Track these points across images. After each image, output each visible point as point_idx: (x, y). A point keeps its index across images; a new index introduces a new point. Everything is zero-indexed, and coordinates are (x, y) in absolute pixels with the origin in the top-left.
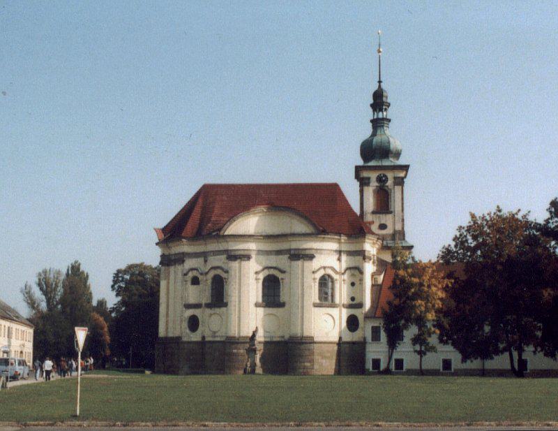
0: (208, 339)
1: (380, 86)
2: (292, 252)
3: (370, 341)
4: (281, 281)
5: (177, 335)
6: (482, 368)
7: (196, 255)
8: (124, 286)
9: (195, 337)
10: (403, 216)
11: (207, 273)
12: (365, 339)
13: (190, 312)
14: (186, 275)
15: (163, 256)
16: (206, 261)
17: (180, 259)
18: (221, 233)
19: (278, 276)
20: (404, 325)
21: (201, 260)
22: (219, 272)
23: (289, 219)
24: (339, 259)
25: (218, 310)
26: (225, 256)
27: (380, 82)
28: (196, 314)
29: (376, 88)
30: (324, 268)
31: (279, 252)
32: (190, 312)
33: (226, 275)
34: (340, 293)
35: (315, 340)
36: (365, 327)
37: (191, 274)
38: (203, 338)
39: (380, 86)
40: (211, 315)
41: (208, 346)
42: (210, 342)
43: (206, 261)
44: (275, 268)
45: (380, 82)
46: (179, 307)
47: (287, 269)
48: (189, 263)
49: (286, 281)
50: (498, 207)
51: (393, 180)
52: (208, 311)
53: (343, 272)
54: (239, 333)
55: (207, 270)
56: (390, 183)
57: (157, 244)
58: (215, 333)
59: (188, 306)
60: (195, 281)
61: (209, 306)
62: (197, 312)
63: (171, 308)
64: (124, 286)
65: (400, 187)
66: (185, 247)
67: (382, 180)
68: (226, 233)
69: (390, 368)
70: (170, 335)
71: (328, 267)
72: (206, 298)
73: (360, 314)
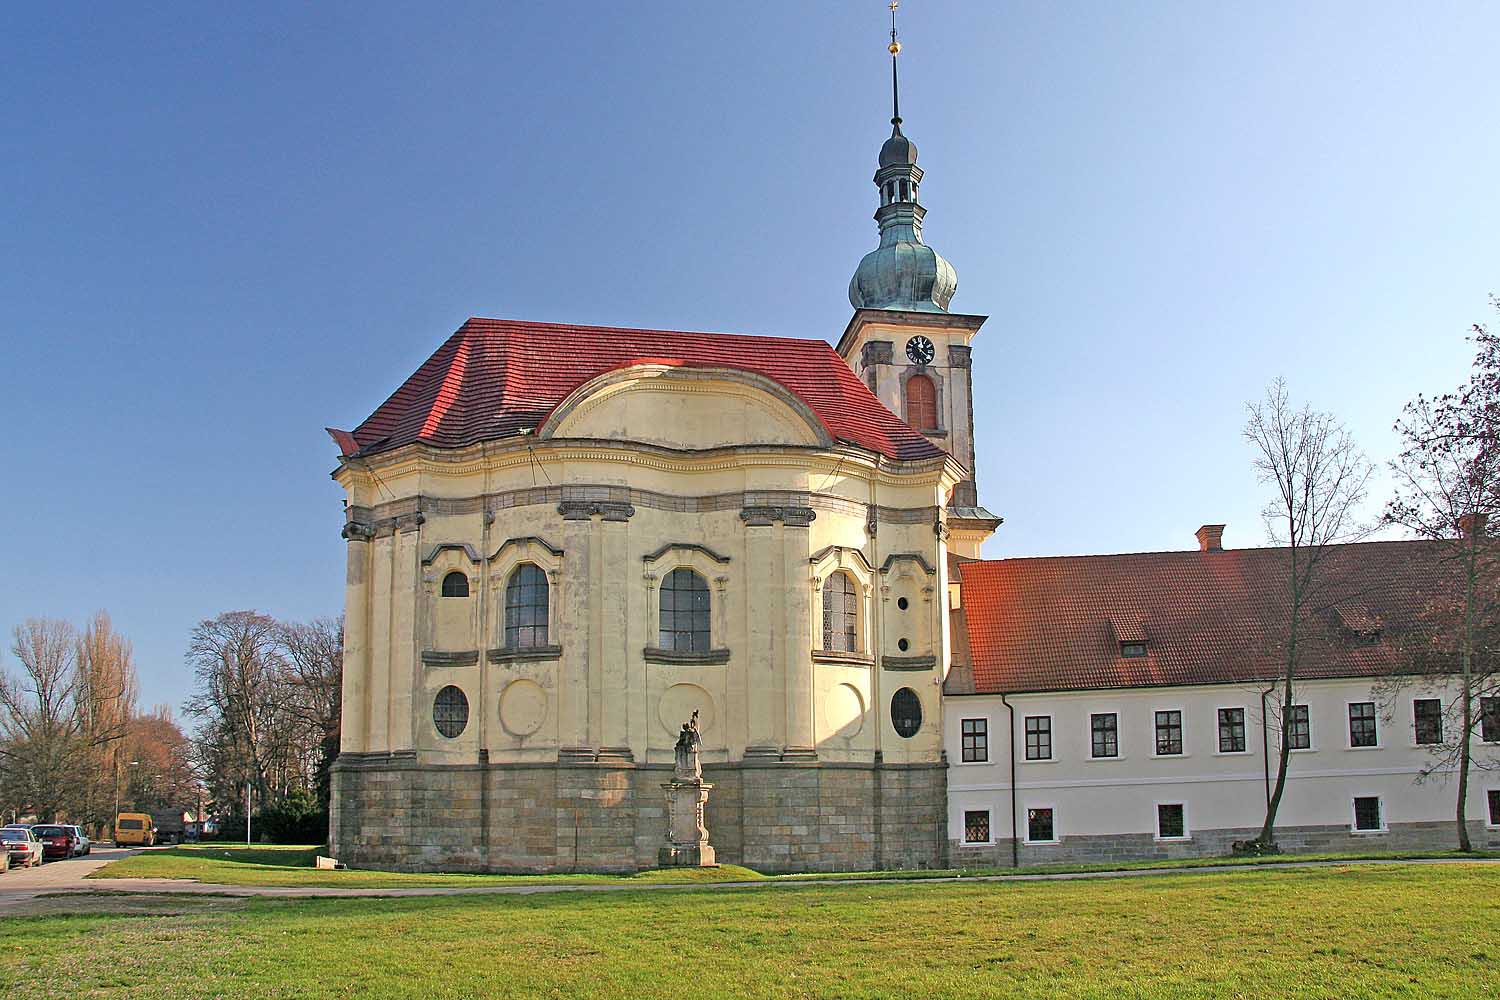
1: (897, 131)
2: (750, 501)
4: (713, 587)
8: (206, 830)
9: (461, 751)
13: (440, 678)
14: (426, 562)
16: (489, 523)
18: (543, 432)
22: (537, 555)
26: (553, 506)
27: (896, 121)
31: (707, 503)
32: (440, 678)
34: (272, 885)
36: (942, 723)
38: (484, 754)
39: (897, 131)
40: (508, 685)
41: (497, 777)
42: (508, 767)
43: (489, 523)
45: (896, 121)
48: (440, 529)
50: (1000, 521)
52: (498, 673)
56: (939, 360)
58: (521, 738)
59: (435, 659)
60: (455, 584)
63: (379, 666)
64: (206, 830)
67: (919, 352)
71: (849, 549)
73: (924, 685)
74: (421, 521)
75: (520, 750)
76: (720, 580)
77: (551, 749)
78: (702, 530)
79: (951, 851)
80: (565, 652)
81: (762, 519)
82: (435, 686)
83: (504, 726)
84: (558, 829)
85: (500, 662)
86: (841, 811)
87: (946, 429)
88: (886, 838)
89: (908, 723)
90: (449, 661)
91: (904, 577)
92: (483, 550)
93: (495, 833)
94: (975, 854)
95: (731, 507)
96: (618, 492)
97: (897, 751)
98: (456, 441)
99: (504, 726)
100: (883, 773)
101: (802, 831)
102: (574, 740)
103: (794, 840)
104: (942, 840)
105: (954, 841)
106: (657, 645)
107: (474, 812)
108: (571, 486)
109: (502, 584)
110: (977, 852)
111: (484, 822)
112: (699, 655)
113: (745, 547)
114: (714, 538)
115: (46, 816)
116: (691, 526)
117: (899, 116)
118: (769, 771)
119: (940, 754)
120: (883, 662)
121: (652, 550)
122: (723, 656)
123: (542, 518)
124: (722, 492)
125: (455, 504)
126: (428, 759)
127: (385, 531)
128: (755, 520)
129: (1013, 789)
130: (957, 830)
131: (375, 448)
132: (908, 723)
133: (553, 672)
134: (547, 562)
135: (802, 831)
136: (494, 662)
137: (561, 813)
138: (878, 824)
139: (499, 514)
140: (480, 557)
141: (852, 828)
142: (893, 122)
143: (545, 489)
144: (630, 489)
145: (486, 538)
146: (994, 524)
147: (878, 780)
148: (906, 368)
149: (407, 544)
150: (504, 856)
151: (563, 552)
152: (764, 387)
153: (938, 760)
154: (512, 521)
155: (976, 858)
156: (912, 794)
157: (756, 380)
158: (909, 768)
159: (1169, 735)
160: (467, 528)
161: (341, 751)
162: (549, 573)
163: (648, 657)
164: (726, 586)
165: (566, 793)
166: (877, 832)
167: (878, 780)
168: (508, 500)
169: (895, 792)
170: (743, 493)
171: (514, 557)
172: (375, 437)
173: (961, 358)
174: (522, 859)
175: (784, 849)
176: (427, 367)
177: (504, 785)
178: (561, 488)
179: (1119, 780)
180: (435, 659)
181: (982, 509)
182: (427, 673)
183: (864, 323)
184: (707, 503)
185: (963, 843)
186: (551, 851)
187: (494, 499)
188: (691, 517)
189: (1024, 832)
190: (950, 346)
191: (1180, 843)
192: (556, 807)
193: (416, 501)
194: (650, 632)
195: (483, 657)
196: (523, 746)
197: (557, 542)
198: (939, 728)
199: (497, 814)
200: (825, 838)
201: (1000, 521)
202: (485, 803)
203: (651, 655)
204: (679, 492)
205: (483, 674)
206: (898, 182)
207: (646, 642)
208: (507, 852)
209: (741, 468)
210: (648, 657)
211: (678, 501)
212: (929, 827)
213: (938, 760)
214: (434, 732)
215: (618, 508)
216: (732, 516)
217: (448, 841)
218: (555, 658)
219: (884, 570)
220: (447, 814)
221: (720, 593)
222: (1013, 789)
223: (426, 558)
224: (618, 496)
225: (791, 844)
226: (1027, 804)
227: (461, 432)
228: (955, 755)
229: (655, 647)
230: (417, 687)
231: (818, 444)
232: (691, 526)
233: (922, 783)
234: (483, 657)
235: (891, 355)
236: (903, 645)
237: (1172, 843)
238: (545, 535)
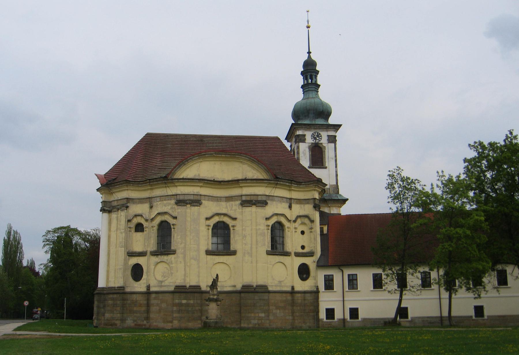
0: (152, 289)
1: (309, 57)
2: (244, 198)
3: (324, 290)
4: (231, 228)
5: (119, 285)
6: (439, 315)
7: (141, 201)
9: (140, 287)
10: (336, 172)
11: (152, 220)
12: (317, 288)
13: (134, 261)
15: (104, 202)
16: (151, 207)
17: (125, 205)
19: (228, 223)
20: (444, 277)
21: (146, 206)
23: (241, 165)
24: (290, 207)
25: (165, 258)
26: (173, 202)
27: (309, 53)
28: (302, 250)
29: (306, 57)
30: (277, 214)
31: (229, 199)
32: (134, 261)
33: (175, 220)
35: (270, 289)
37: (136, 221)
38: (148, 287)
43: (151, 207)
44: (225, 215)
45: (309, 53)
46: (122, 253)
47: (238, 216)
48: (135, 209)
49: (238, 228)
50: (347, 200)
51: (327, 138)
53: (294, 219)
54: (447, 298)
55: (153, 216)
57: (98, 190)
58: (162, 282)
59: (131, 254)
60: (139, 228)
61: (154, 254)
62: (141, 261)
65: (333, 145)
66: (122, 194)
68: (175, 177)
69: (346, 317)
70: (112, 285)
72: (152, 245)
74: (127, 207)
75: (161, 286)
76: (233, 226)
77: (172, 286)
78: (227, 208)
79: (320, 323)
80: (177, 252)
81: (248, 205)
82: (132, 263)
83: (155, 278)
84: (174, 314)
85: (154, 255)
86: (278, 308)
87: (326, 166)
88: (296, 318)
89: (305, 276)
90: (137, 255)
91: (303, 223)
92: (149, 216)
93: (152, 315)
94: (329, 324)
95: (237, 200)
96: (196, 196)
97: (301, 286)
98: (140, 179)
99: (155, 278)
100: (294, 294)
101: (263, 315)
102: (179, 281)
103: (260, 319)
104: (317, 318)
105: (322, 319)
106: (210, 249)
107: (143, 309)
108: (179, 195)
109: (156, 229)
110: (330, 324)
111: (148, 311)
112: (225, 252)
113: (242, 214)
114: (232, 211)
115: (440, 228)
116: (223, 207)
117: (310, 51)
118: (137, 295)
119: (316, 287)
120: (295, 254)
121: (209, 215)
122: (234, 253)
123: (168, 206)
124: (234, 195)
125: (140, 200)
126: (128, 290)
127: (115, 210)
128: (246, 205)
129: (344, 301)
130: (323, 315)
131: (112, 181)
132: (305, 276)
133: (173, 259)
134: (171, 221)
135: (263, 315)
136: (152, 255)
137: (175, 308)
138: (293, 312)
139: (155, 204)
140: (148, 219)
141: (282, 314)
142: (308, 53)
143: (171, 195)
144: (201, 195)
145: (150, 212)
146: (344, 201)
147: (293, 297)
148: (311, 144)
149: (122, 215)
150: (155, 324)
151: (176, 217)
152: (248, 159)
153: (315, 290)
154: (160, 207)
155: (329, 326)
156: (306, 302)
157: (246, 156)
158: (305, 292)
159: (353, 282)
160: (142, 209)
161: (98, 287)
162: (172, 225)
163: (207, 253)
164: (235, 228)
165: (177, 301)
166: (292, 315)
167: (293, 297)
168: (158, 199)
169: (300, 301)
170: (242, 196)
171: (159, 219)
172: (112, 177)
173: (332, 140)
174: (161, 325)
175: (256, 322)
176: (133, 149)
177: (155, 298)
178: (176, 195)
179: (375, 298)
180: (131, 254)
181: (340, 195)
182: (129, 259)
183: (295, 128)
184: (229, 199)
185: (325, 320)
186: (171, 322)
187: (153, 199)
188: (223, 204)
189: (348, 316)
190: (328, 135)
191: (406, 321)
192: (173, 306)
193: (126, 200)
194: (208, 244)
195: (148, 253)
196: (162, 285)
197: (174, 214)
198: (315, 278)
199: (153, 309)
200: (271, 318)
201: (347, 200)
202: (148, 305)
203: (209, 253)
204: (218, 196)
205: (148, 260)
206: (309, 75)
207: (207, 248)
208: (156, 322)
209: (241, 187)
210: (207, 253)
211: (218, 198)
212: (312, 314)
213: (315, 290)
214: (131, 279)
215: (196, 202)
216: (238, 203)
217: (135, 318)
218: (174, 254)
219: (295, 221)
220: (135, 309)
221: (233, 231)
222: (344, 301)
223: (129, 218)
224: (196, 198)
225: (258, 320)
226: (349, 305)
227: (142, 176)
228: (322, 287)
229: (209, 249)
230: (126, 263)
231: (268, 179)
232: (223, 207)
233: (308, 297)
234: (148, 253)
235: (305, 139)
236: (303, 247)
237: (404, 321)
238: (170, 212)
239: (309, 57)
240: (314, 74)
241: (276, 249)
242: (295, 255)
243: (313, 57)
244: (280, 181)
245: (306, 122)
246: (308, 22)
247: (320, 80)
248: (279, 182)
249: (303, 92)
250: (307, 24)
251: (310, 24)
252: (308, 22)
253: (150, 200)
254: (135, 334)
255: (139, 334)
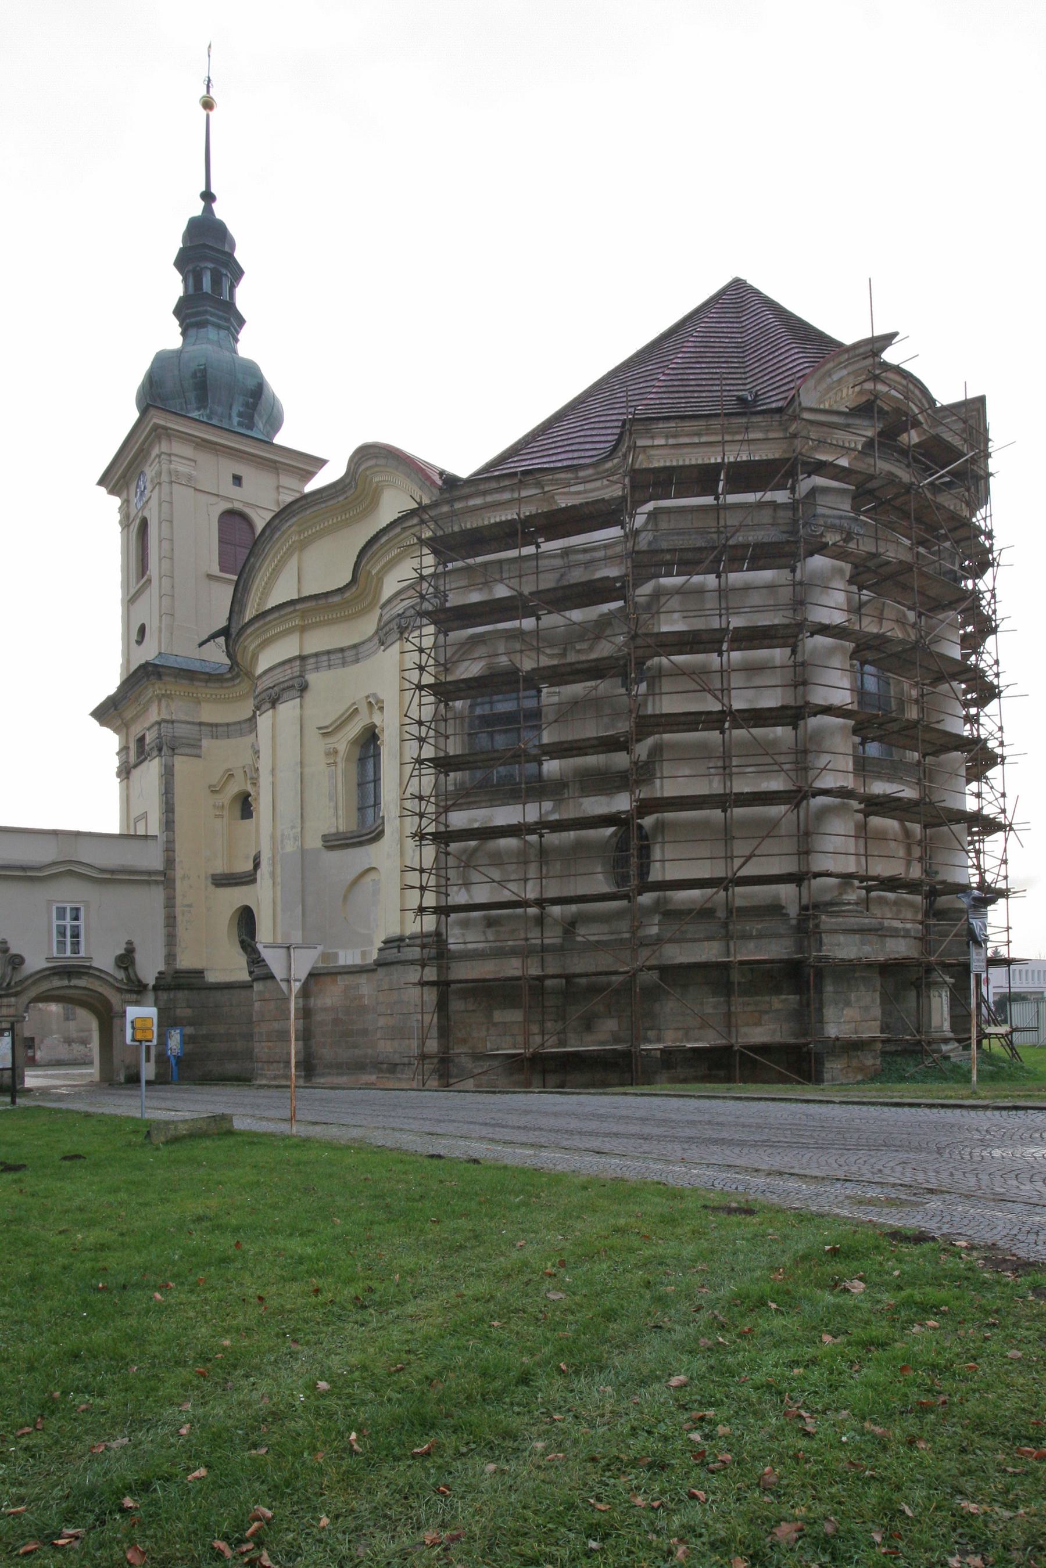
1: (208, 210)
27: (208, 197)
29: (197, 208)
45: (208, 197)
239: (208, 210)
240: (210, 265)
241: (64, 909)
242: (213, 884)
243: (220, 211)
244: (467, 497)
245: (651, 588)
246: (208, 87)
247: (244, 298)
248: (458, 505)
249: (180, 330)
250: (211, 114)
251: (213, 93)
252: (208, 87)
253: (343, 658)
254: (934, 1098)
255: (812, 983)
